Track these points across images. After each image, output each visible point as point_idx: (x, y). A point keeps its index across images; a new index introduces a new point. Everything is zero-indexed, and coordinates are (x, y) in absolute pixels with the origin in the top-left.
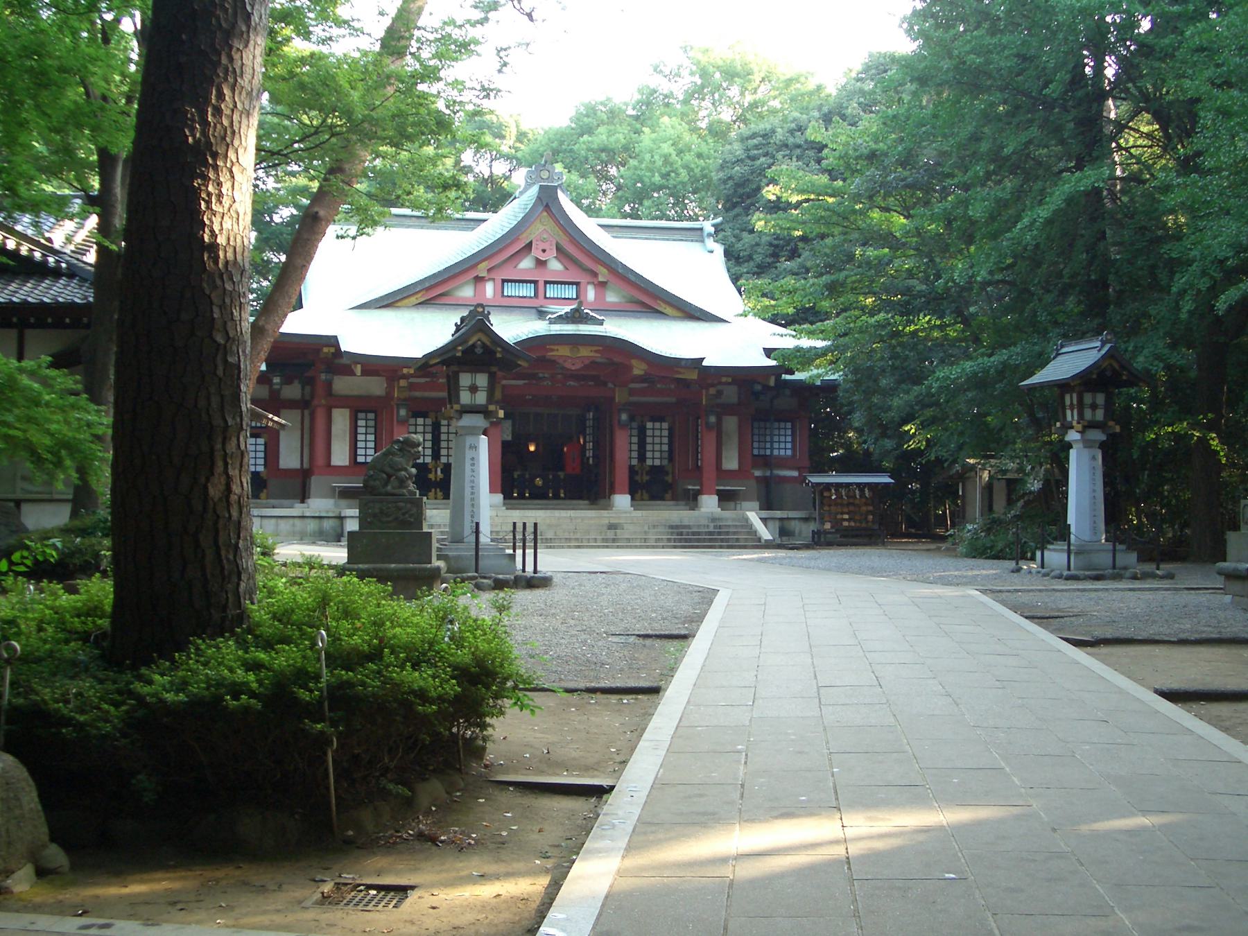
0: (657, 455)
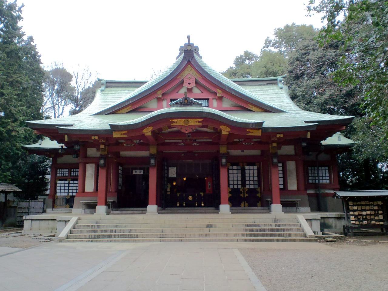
0: (252, 183)
